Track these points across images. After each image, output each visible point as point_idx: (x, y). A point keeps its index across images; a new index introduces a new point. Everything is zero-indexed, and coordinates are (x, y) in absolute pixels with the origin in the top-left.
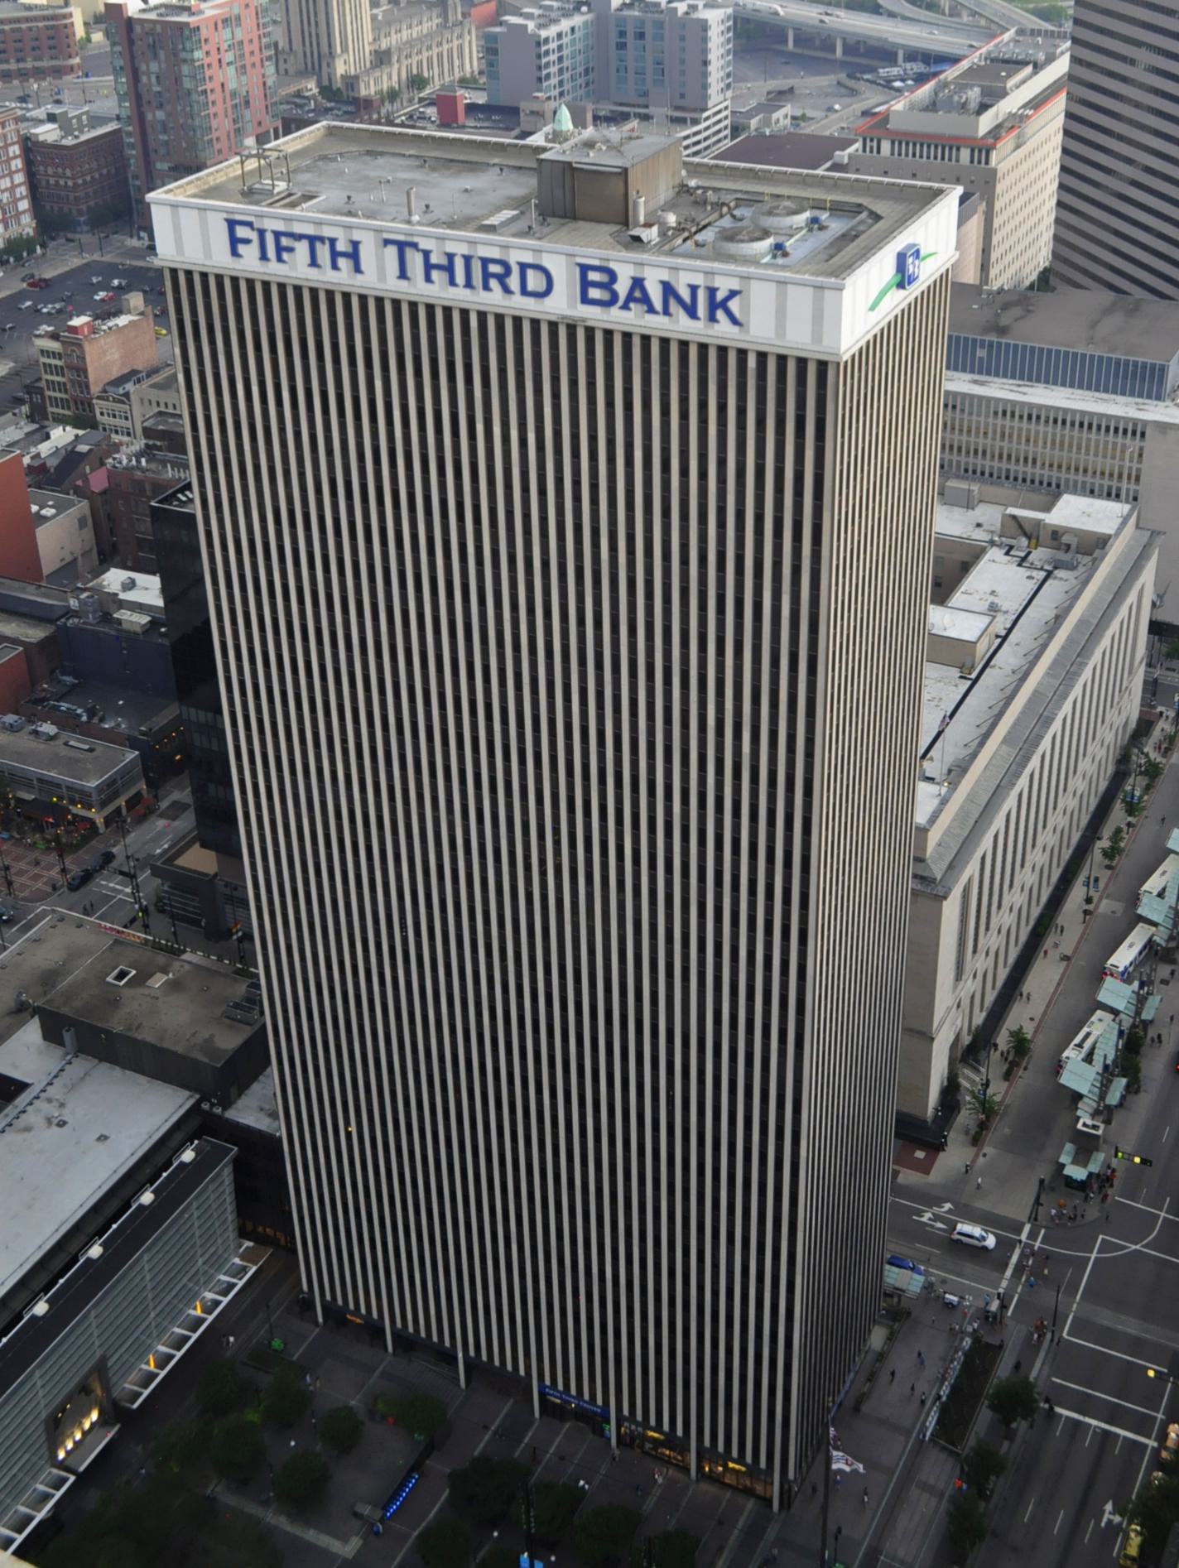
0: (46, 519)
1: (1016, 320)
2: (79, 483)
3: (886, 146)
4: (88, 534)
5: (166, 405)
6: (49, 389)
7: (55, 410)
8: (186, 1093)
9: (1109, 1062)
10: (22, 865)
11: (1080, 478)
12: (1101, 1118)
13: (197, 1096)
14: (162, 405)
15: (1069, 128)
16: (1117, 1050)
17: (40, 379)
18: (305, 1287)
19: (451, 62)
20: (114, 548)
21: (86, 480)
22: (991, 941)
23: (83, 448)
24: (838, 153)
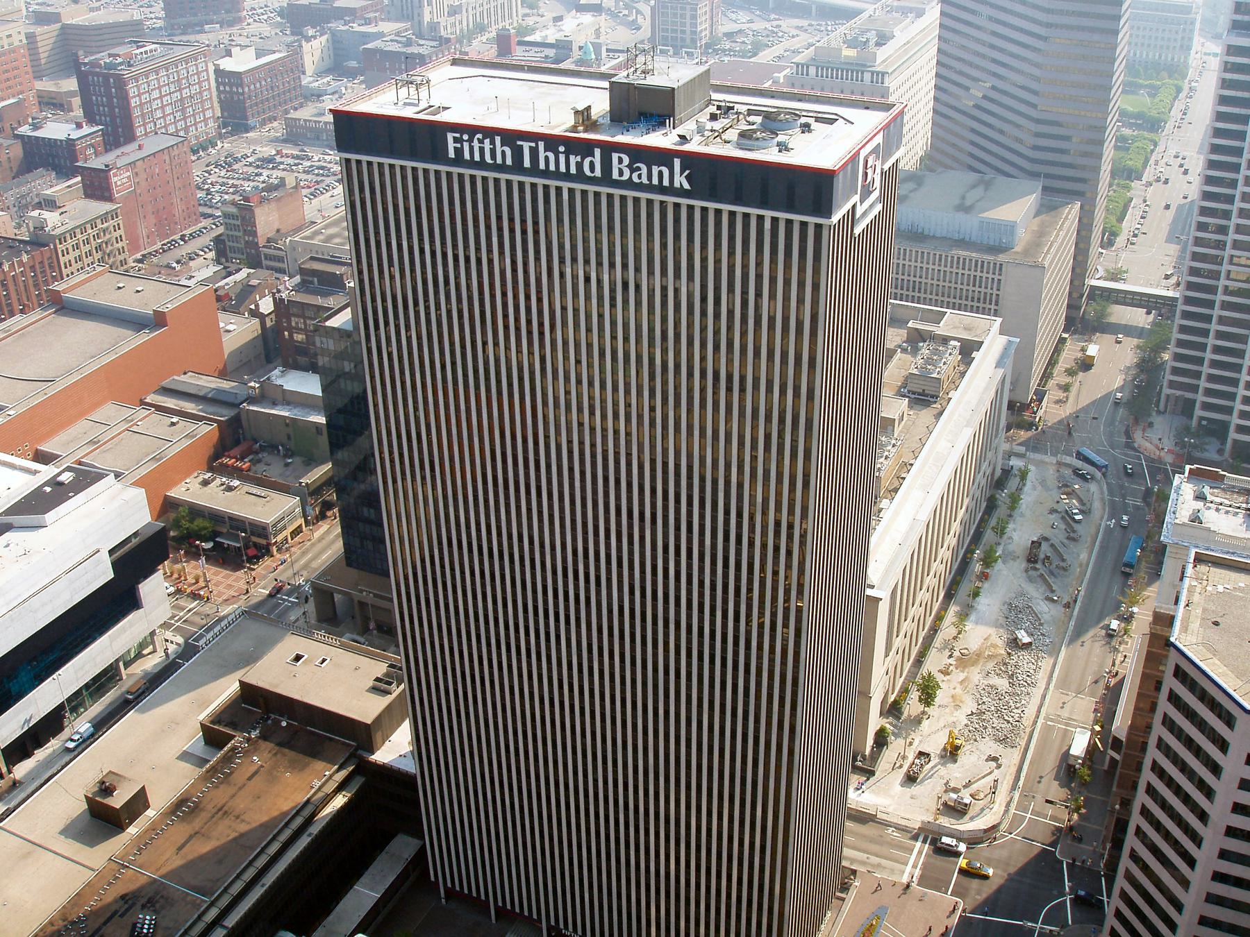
1: (911, 191)
2: (253, 307)
6: (229, 241)
7: (231, 244)
10: (219, 578)
15: (940, 72)
18: (432, 878)
21: (257, 306)
22: (907, 626)
23: (254, 282)
24: (776, 75)
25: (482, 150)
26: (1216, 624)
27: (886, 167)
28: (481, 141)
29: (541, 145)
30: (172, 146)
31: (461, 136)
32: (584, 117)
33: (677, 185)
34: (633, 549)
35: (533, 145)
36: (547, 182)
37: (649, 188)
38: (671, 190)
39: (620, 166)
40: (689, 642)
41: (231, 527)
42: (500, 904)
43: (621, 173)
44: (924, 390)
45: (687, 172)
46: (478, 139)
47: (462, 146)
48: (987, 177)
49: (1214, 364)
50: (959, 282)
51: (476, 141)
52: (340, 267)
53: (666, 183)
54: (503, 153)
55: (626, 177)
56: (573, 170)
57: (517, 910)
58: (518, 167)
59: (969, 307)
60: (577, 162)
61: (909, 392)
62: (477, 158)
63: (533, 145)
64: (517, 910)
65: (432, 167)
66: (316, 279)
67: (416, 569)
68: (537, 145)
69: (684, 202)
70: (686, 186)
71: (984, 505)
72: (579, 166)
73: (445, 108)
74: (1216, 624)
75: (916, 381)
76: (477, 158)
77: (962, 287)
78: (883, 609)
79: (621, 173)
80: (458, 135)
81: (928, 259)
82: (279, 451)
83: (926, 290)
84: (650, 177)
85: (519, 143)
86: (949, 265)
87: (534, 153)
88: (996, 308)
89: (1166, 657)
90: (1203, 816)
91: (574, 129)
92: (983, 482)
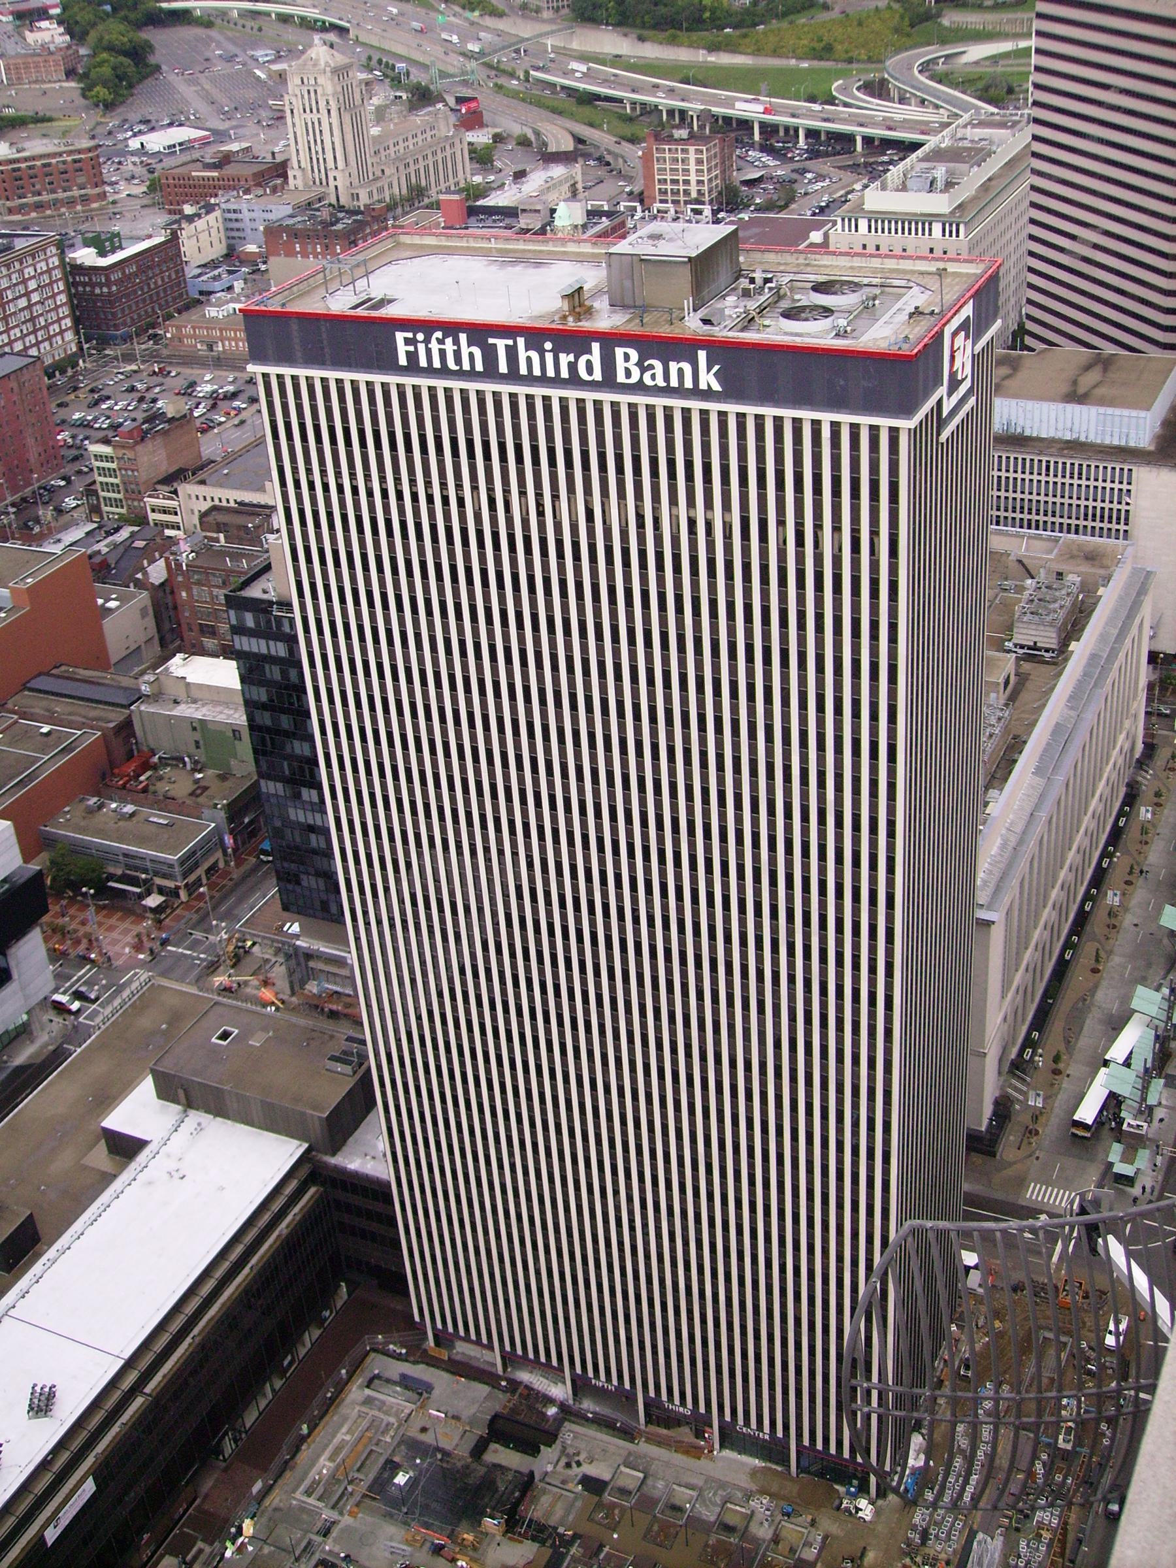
0: (110, 610)
2: (139, 576)
3: (863, 224)
4: (150, 622)
5: (228, 501)
8: (296, 1142)
9: (1149, 1065)
11: (1114, 526)
12: (1144, 1117)
13: (306, 1145)
14: (209, 499)
16: (1154, 1053)
17: (94, 482)
18: (417, 1318)
19: (454, 164)
20: (178, 633)
21: (145, 574)
25: (442, 353)
27: (978, 348)
28: (441, 341)
29: (521, 342)
30: (21, 369)
31: (415, 335)
32: (576, 298)
33: (703, 386)
34: (665, 870)
35: (510, 342)
36: (723, 407)
37: (667, 391)
38: (696, 393)
39: (627, 365)
41: (128, 867)
42: (508, 1348)
43: (628, 374)
44: (1035, 643)
45: (716, 368)
46: (437, 339)
47: (416, 348)
50: (1075, 496)
51: (434, 340)
52: (252, 518)
53: (688, 384)
54: (471, 355)
55: (634, 379)
56: (565, 374)
57: (519, 1352)
58: (490, 372)
59: (1089, 529)
60: (569, 363)
61: (1016, 645)
62: (437, 364)
63: (510, 342)
64: (519, 1352)
65: (378, 379)
66: (222, 536)
67: (405, 915)
68: (515, 342)
69: (714, 407)
70: (716, 387)
71: (1123, 790)
72: (573, 367)
73: (390, 301)
75: (1025, 631)
76: (437, 364)
77: (1070, 501)
78: (997, 935)
79: (628, 374)
80: (410, 335)
81: (1113, 476)
82: (185, 763)
84: (667, 377)
85: (491, 341)
86: (1060, 474)
87: (512, 352)
88: (1126, 528)
92: (1120, 761)
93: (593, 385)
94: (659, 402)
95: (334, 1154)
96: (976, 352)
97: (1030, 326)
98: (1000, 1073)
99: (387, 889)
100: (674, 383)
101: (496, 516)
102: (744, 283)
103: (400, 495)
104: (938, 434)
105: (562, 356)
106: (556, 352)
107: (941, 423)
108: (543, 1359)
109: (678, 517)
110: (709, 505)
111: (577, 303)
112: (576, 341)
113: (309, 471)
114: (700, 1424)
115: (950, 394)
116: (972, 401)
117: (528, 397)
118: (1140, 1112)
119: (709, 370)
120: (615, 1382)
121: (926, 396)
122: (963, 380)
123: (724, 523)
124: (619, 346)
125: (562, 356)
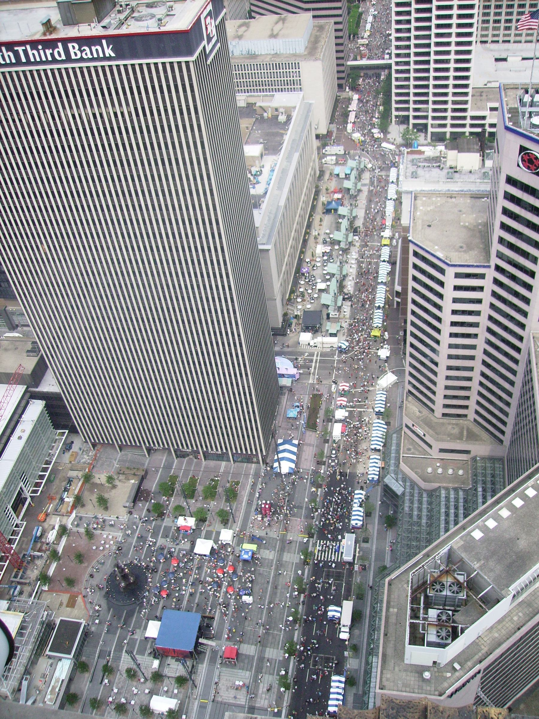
1: (244, 32)
11: (261, 88)
26: (429, 226)
27: (217, 22)
29: (28, 47)
32: (48, 26)
33: (107, 55)
35: (24, 48)
37: (93, 59)
40: (176, 293)
42: (120, 443)
43: (76, 54)
45: (111, 46)
48: (283, 16)
49: (416, 94)
55: (79, 56)
56: (50, 59)
57: (125, 443)
58: (19, 62)
60: (51, 54)
63: (24, 48)
68: (26, 48)
70: (113, 55)
72: (52, 55)
74: (429, 226)
78: (272, 255)
79: (76, 54)
83: (272, 84)
84: (92, 53)
85: (16, 48)
87: (25, 52)
89: (408, 247)
90: (439, 320)
91: (44, 34)
92: (311, 179)
93: (62, 62)
94: (91, 64)
95: (37, 388)
96: (217, 24)
97: (253, 8)
98: (283, 305)
99: (35, 282)
100: (95, 56)
101: (184, 117)
102: (118, 8)
103: (14, 121)
104: (206, 61)
105: (47, 51)
106: (43, 49)
107: (207, 57)
108: (134, 444)
109: (109, 113)
110: (120, 105)
111: (49, 26)
112: (51, 44)
113: (11, 114)
114: (196, 453)
115: (208, 43)
116: (219, 45)
117: (87, 67)
118: (335, 309)
119: (108, 48)
120: (162, 446)
121: (198, 46)
122: (213, 37)
123: (128, 112)
124: (70, 43)
125: (47, 51)
